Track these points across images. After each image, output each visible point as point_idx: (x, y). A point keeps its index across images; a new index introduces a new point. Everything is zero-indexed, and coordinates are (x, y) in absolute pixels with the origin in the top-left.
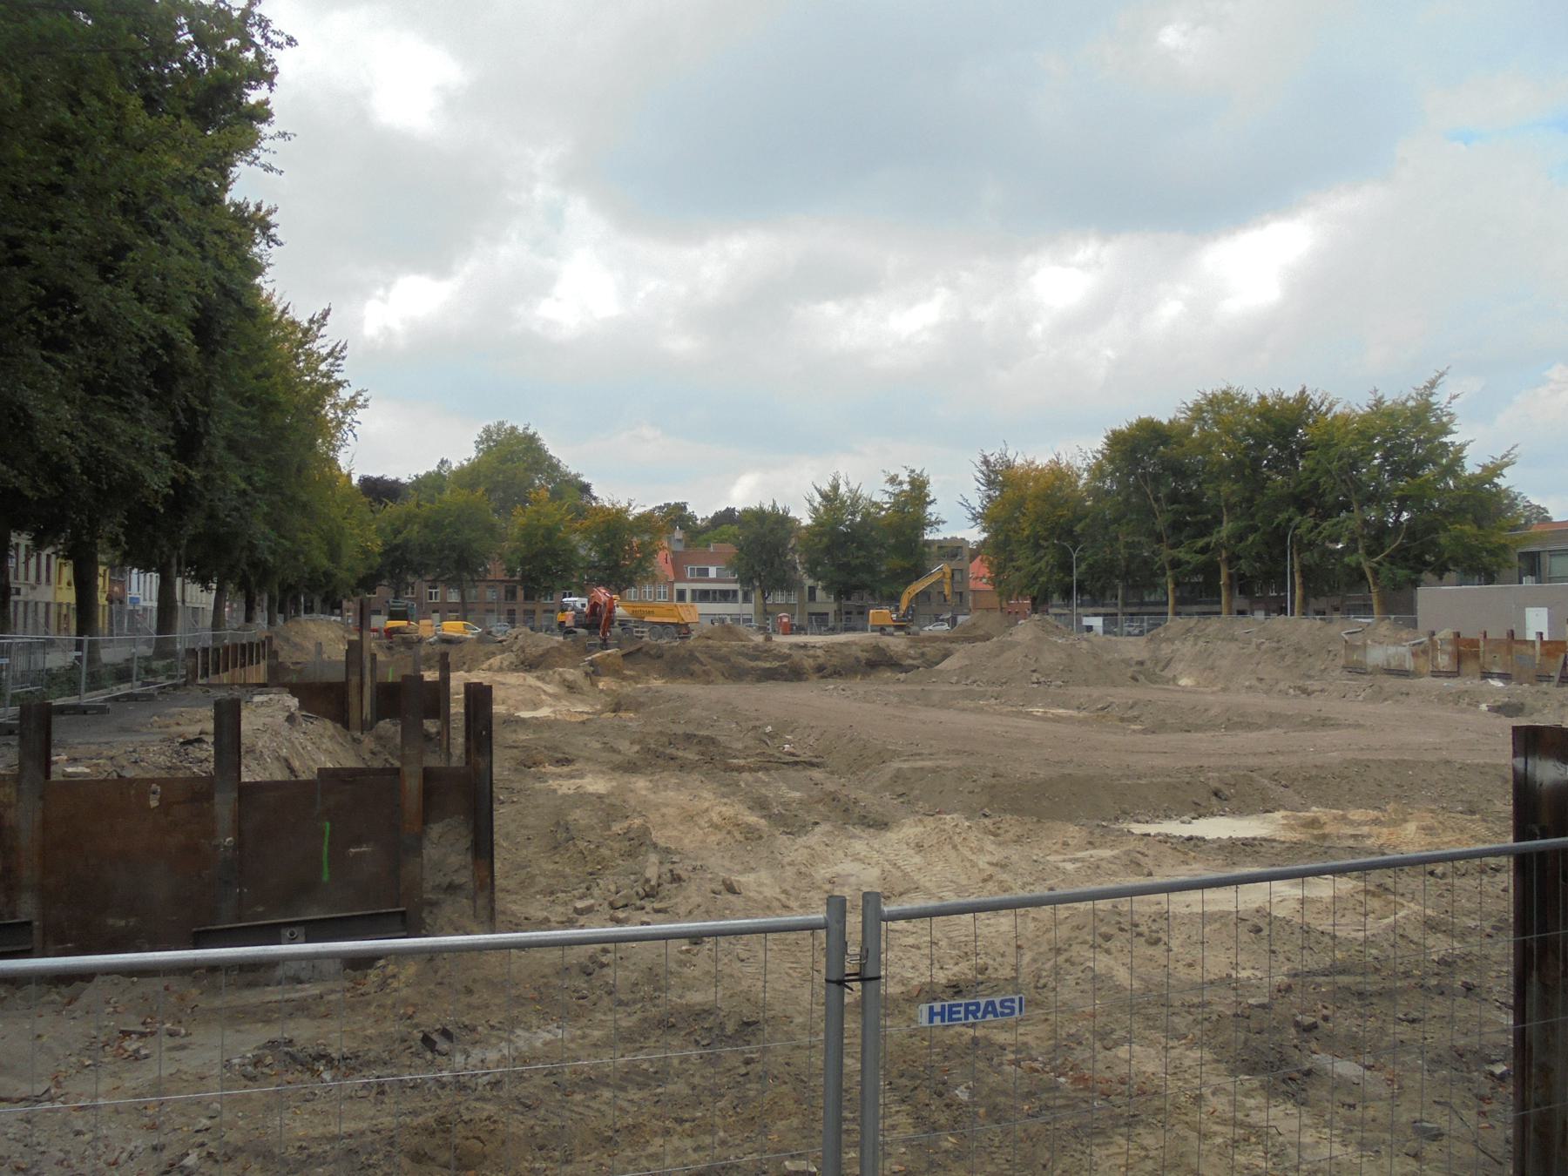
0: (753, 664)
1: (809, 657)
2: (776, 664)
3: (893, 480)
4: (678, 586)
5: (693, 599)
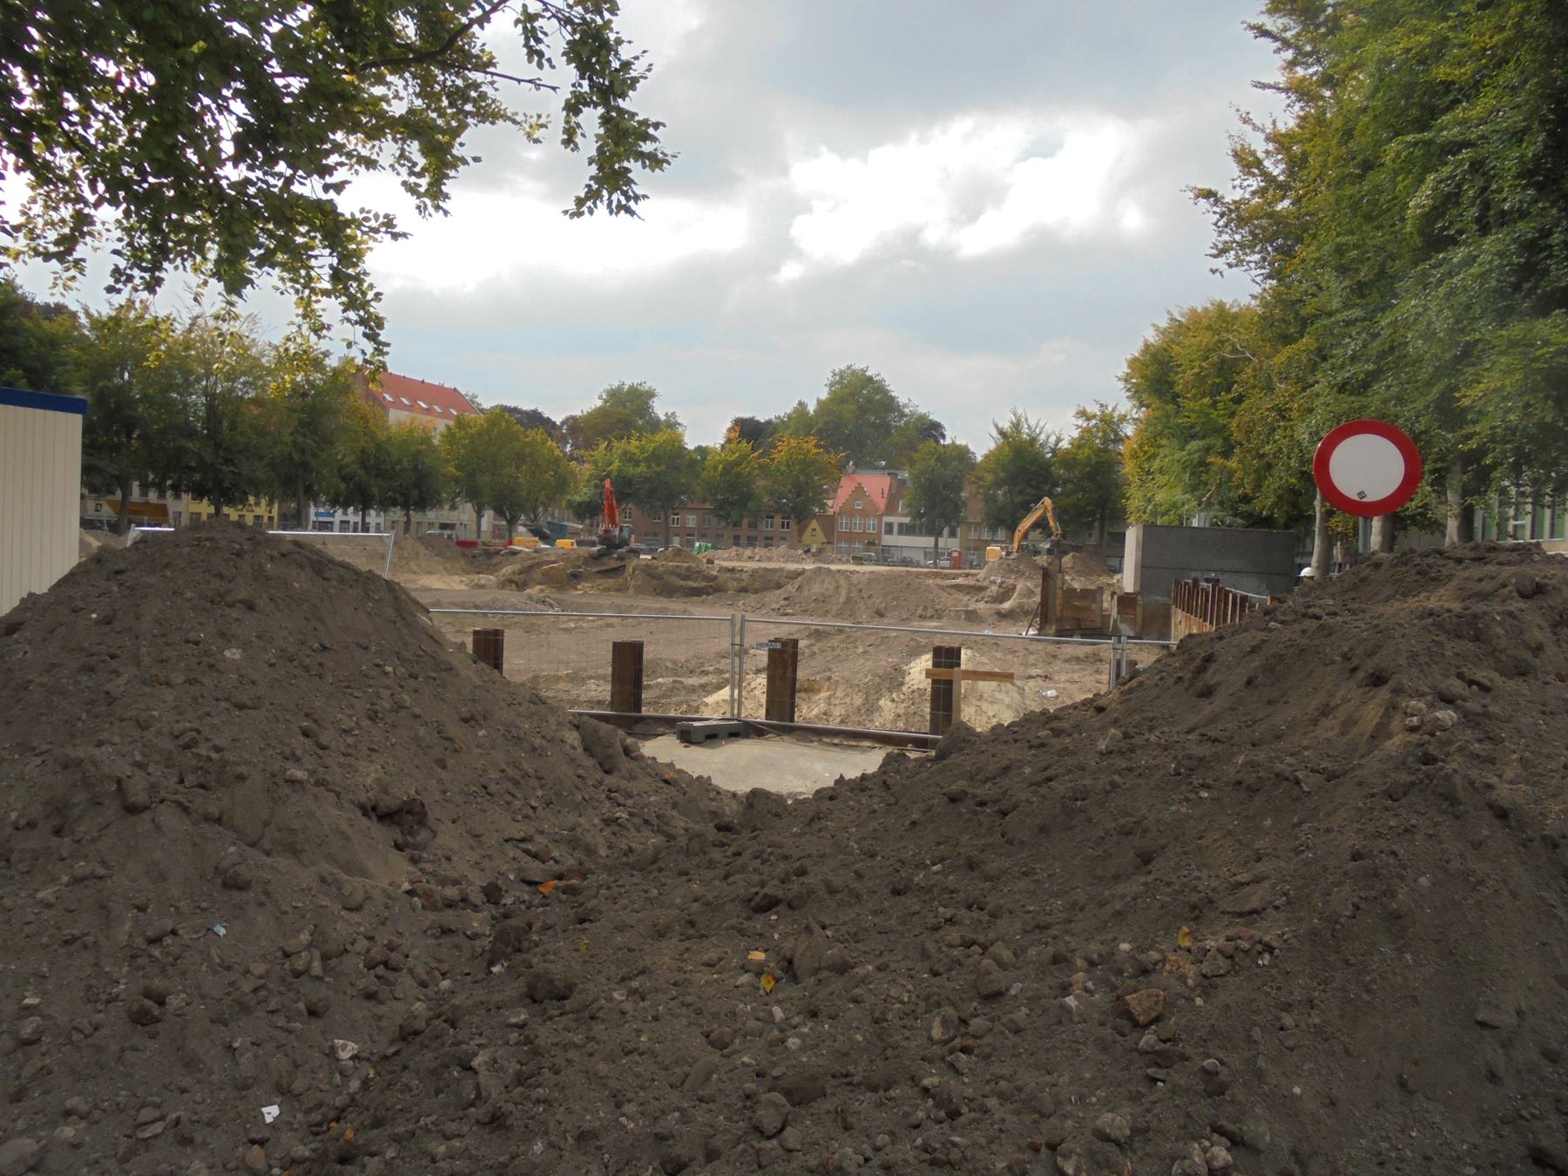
0: (683, 583)
1: (734, 579)
2: (703, 584)
3: (1083, 414)
4: (886, 519)
5: (900, 533)
